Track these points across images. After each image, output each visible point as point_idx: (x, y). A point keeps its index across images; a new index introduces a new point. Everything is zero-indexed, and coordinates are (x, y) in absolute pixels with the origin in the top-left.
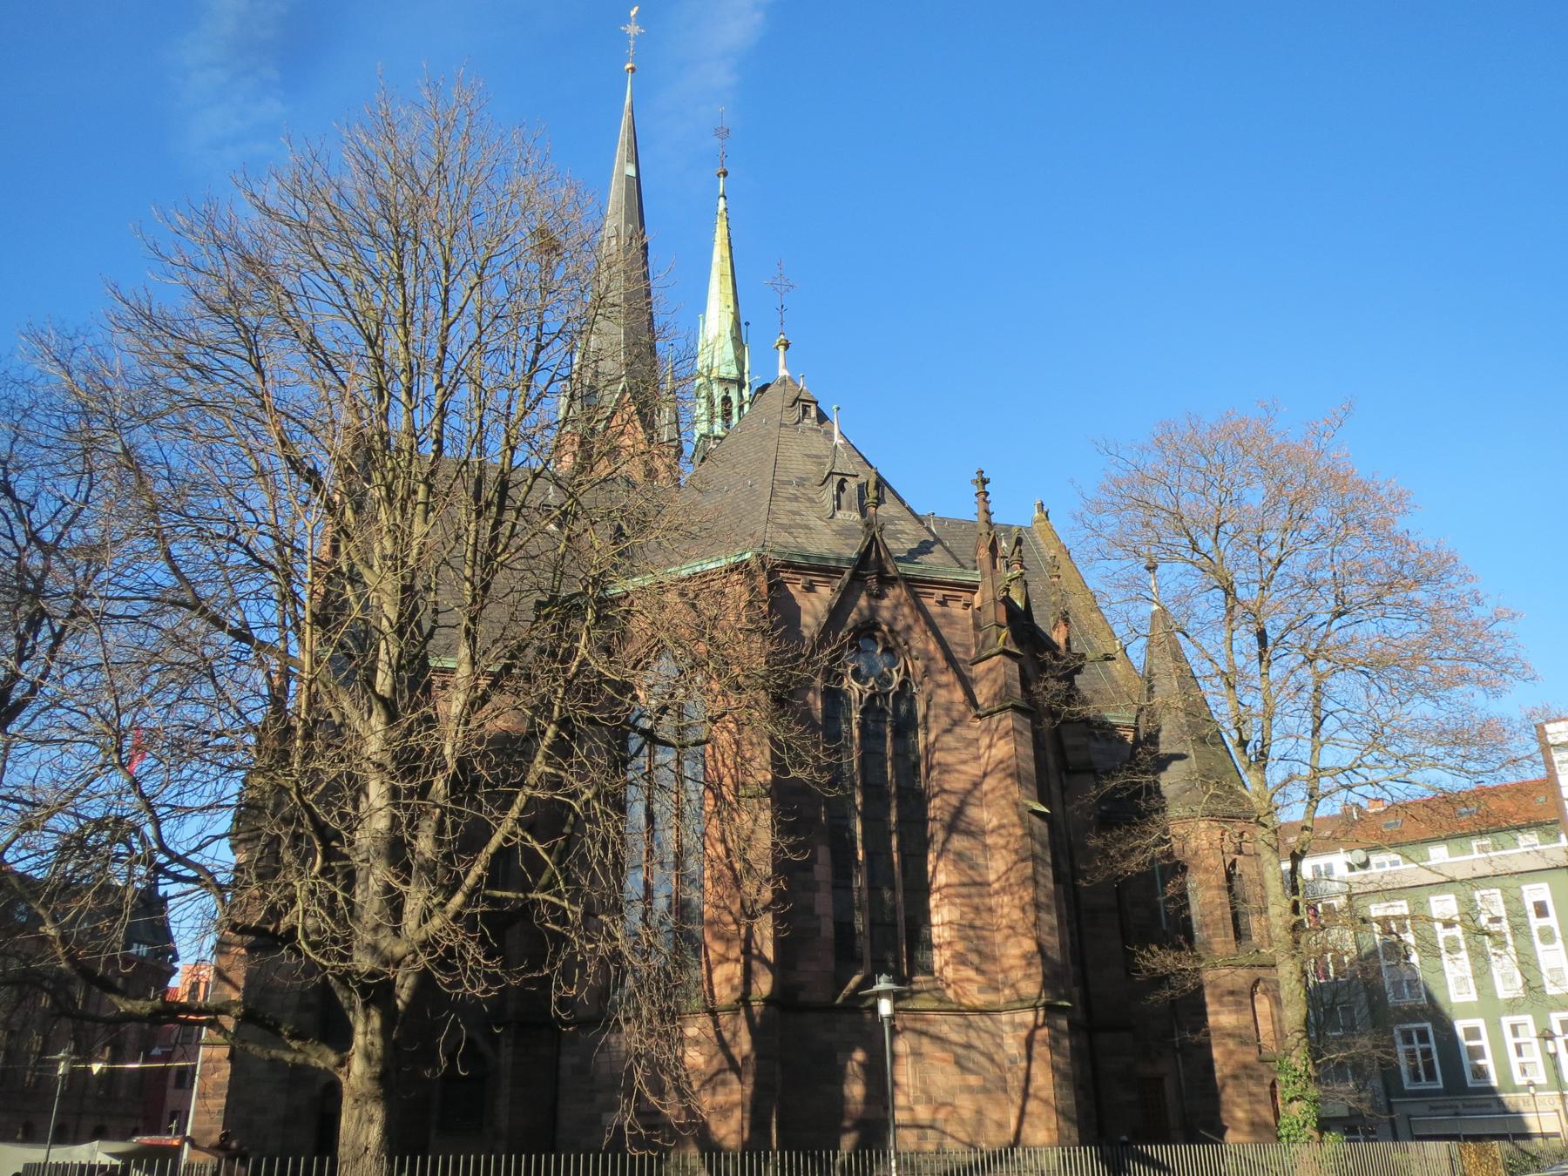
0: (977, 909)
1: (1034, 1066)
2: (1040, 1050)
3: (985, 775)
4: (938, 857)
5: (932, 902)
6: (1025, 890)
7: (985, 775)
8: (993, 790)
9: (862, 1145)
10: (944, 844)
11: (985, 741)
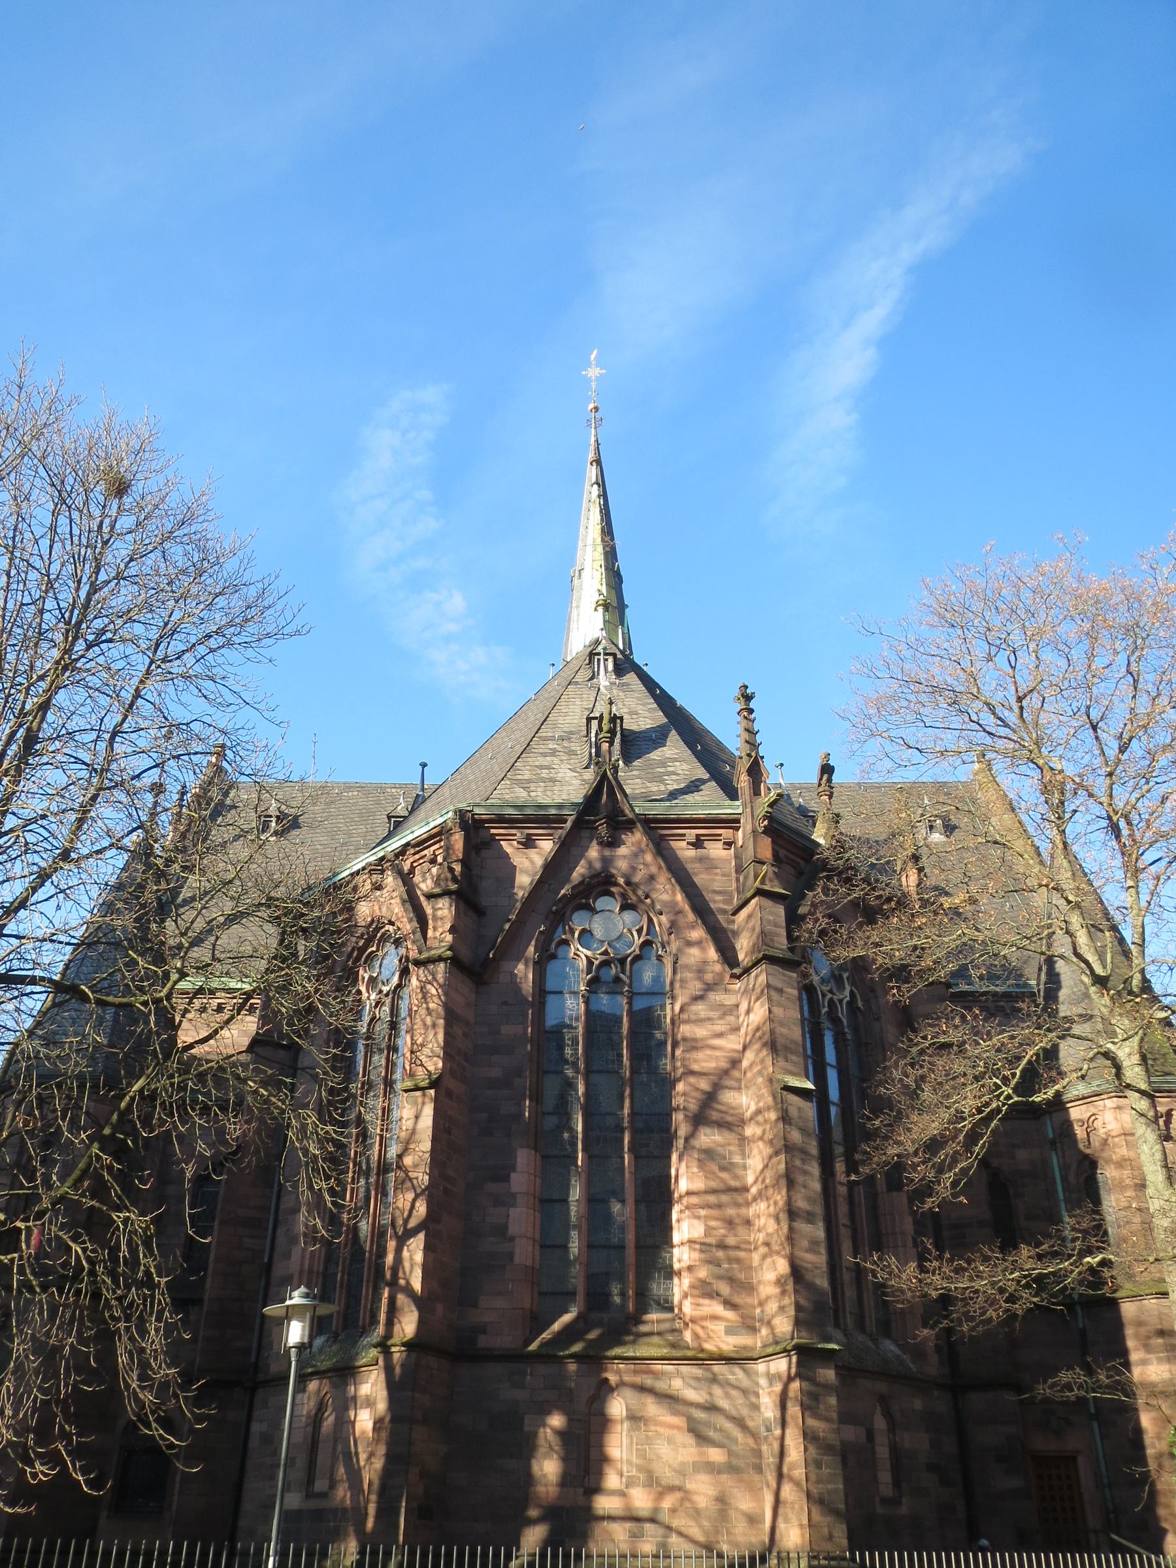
0: (730, 1223)
1: (788, 1432)
2: (794, 1410)
3: (745, 1048)
4: (680, 1158)
5: (675, 1216)
6: (779, 1193)
7: (745, 1048)
8: (751, 1065)
9: (552, 1541)
10: (687, 1140)
11: (744, 1006)
